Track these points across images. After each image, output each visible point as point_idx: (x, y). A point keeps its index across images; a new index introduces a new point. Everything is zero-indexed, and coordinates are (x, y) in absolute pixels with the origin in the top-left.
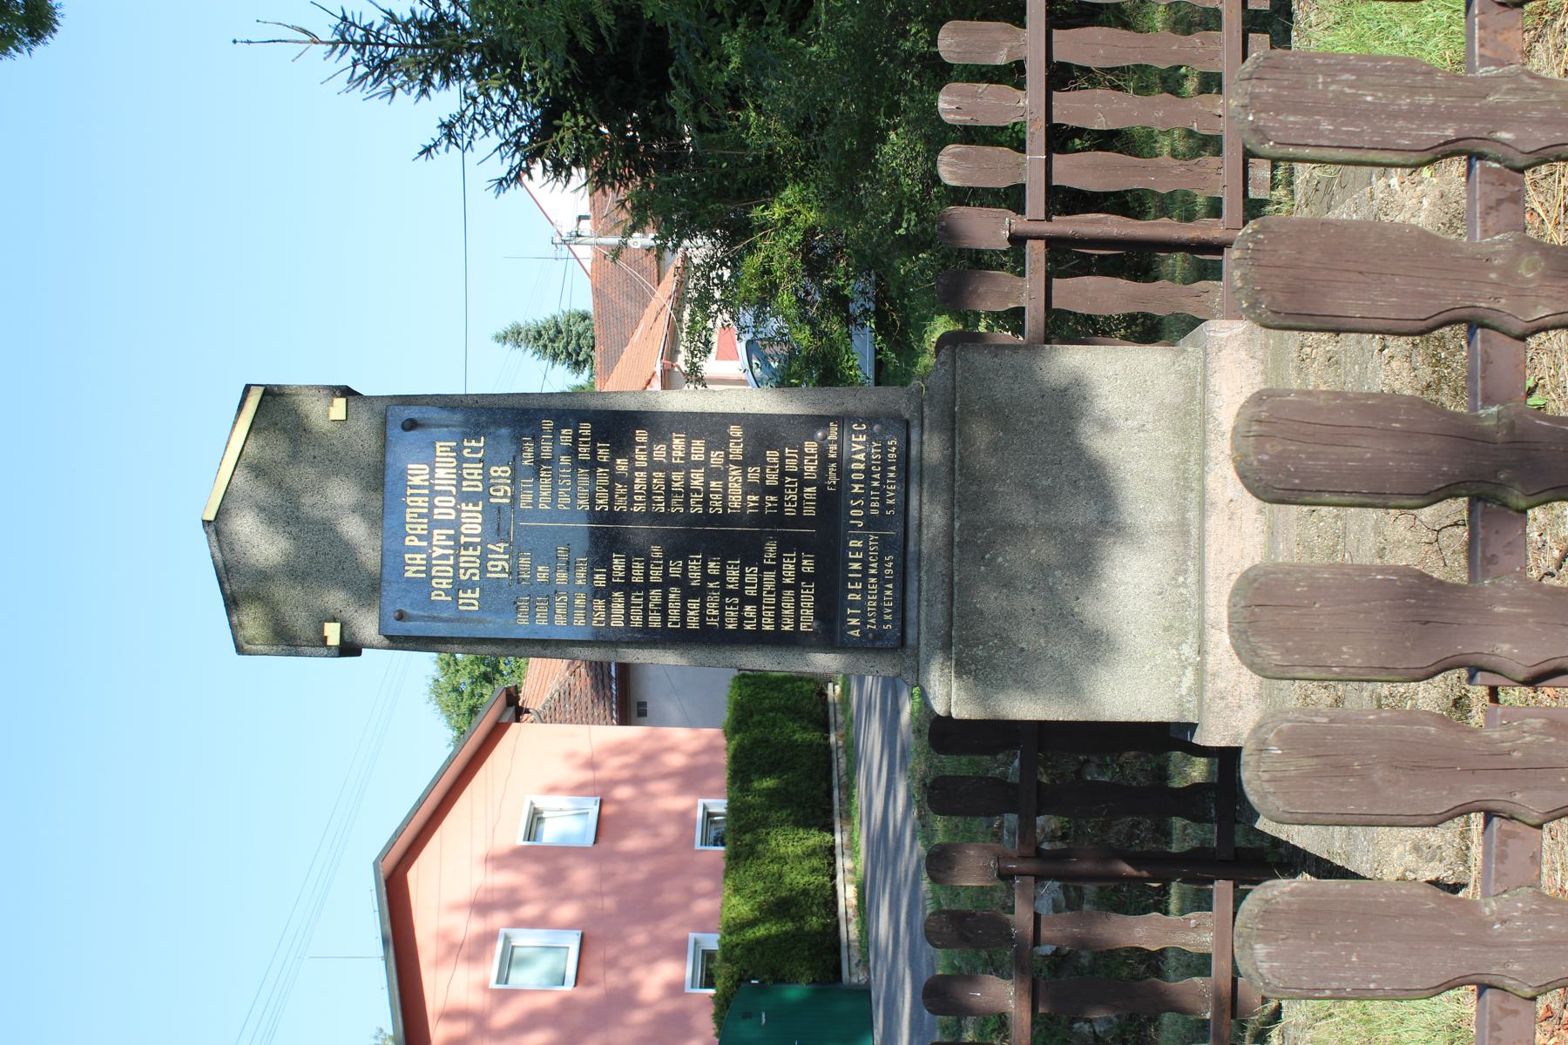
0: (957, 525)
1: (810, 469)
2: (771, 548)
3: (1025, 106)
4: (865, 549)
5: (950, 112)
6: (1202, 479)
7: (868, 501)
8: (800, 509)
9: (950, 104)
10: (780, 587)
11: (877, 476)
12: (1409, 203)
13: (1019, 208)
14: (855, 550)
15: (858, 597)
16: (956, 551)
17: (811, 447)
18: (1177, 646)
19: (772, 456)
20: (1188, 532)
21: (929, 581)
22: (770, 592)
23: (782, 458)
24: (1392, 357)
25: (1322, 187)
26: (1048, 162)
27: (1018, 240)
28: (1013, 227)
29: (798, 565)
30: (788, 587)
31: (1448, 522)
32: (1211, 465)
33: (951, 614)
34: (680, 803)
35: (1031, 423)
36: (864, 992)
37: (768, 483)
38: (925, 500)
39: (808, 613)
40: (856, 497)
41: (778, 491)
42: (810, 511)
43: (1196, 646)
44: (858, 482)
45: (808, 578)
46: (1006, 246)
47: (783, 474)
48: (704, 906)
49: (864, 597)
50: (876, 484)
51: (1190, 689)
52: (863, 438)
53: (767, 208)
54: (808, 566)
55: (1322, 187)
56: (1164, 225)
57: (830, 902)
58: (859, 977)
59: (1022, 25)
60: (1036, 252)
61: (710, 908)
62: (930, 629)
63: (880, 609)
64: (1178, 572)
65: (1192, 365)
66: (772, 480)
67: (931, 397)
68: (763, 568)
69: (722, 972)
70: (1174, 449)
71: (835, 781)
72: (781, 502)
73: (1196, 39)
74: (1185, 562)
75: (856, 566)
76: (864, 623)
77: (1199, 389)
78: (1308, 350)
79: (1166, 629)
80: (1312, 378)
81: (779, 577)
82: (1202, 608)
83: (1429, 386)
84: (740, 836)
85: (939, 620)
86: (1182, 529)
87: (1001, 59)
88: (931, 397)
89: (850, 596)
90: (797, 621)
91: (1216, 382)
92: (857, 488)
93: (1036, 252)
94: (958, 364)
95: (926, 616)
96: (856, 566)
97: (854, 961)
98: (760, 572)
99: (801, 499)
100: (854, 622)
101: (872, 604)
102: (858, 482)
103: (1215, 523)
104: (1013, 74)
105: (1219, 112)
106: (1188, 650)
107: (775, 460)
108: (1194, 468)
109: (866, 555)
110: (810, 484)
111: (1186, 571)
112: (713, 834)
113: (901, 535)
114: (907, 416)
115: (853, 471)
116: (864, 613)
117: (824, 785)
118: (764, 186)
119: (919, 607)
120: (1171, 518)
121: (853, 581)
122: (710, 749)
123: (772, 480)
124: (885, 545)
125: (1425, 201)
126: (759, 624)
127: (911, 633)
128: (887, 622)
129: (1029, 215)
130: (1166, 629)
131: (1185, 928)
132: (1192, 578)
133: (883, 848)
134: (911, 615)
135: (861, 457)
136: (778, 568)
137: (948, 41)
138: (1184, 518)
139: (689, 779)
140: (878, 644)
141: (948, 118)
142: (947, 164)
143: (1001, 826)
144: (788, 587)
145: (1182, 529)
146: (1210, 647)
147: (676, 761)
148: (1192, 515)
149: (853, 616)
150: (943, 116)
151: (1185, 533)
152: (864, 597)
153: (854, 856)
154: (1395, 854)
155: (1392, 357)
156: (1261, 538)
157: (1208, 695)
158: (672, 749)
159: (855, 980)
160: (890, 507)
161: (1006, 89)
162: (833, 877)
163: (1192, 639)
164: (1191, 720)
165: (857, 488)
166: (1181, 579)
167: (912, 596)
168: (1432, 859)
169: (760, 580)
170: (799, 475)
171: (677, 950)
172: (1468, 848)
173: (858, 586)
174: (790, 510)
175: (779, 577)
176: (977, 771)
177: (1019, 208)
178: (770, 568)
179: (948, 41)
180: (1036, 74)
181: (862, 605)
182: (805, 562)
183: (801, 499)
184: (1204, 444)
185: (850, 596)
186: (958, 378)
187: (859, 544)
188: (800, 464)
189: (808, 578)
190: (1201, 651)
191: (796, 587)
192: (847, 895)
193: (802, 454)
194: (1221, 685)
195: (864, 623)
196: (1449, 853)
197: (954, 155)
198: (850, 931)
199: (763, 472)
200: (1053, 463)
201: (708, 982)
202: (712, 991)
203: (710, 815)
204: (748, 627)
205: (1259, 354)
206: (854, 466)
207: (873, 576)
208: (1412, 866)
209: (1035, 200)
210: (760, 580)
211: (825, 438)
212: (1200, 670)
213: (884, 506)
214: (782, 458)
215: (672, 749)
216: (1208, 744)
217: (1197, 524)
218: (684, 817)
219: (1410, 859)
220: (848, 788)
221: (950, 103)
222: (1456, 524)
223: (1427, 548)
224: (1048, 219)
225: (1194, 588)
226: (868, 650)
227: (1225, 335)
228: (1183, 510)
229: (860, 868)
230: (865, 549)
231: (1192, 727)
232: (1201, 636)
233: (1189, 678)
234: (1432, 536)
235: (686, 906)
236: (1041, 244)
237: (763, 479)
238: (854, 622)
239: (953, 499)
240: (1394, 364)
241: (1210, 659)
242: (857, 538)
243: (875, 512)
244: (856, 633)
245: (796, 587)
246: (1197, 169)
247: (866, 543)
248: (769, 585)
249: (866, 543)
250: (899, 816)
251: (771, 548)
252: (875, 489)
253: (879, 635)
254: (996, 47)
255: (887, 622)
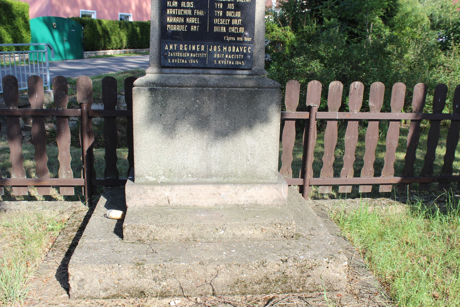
0: (210, 89)
1: (233, 30)
2: (201, 13)
3: (355, 112)
4: (200, 52)
5: (354, 86)
6: (228, 183)
7: (220, 53)
8: (217, 25)
9: (378, 87)
10: (185, 17)
11: (230, 57)
12: (338, 269)
13: (320, 110)
14: (200, 48)
15: (181, 49)
16: (200, 89)
17: (242, 30)
18: (164, 174)
19: (238, 14)
20: (208, 178)
21: (188, 77)
22: (183, 12)
23: (237, 18)
24: (279, 265)
25: (323, 212)
26: (336, 120)
27: (309, 109)
28: (314, 108)
29: (194, 24)
30: (185, 20)
31: (214, 288)
32: (234, 187)
33: (175, 87)
34: (133, 7)
35: (250, 118)
36: (82, 57)
37: (227, 12)
38: (220, 76)
39: (174, 28)
40: (222, 48)
41: (224, 16)
42: (216, 29)
43: (164, 181)
44: (227, 49)
45: (189, 28)
46: (307, 105)
47: (231, 18)
48: (106, 12)
49: (181, 51)
50: (227, 56)
51: (148, 179)
52: (245, 51)
53: (290, 31)
54: (194, 28)
55: (323, 212)
56: (312, 159)
57: (105, 48)
58: (85, 56)
59: (382, 111)
60: (304, 115)
61: (106, 16)
62: (168, 78)
63: (176, 58)
64: (192, 174)
65: (271, 178)
66: (229, 14)
67: (260, 79)
68: (193, 10)
69: (87, 18)
70: (239, 172)
71: (138, 50)
72: (220, 17)
73: (372, 169)
74: (196, 177)
75: (194, 48)
76: (171, 51)
77: (262, 181)
78: (279, 226)
79: (170, 170)
80: (268, 228)
81: (189, 16)
82: (179, 184)
83: (268, 279)
84: (123, 24)
85: (172, 82)
86: (209, 176)
87: (371, 104)
88: (260, 79)
89: (181, 45)
90: (171, 24)
91: (265, 188)
92: (225, 48)
93: (304, 115)
94: (274, 90)
95: (174, 77)
96: (194, 48)
97: (90, 55)
98: (191, 8)
99: (221, 26)
100: (171, 47)
101: (178, 54)
102: (227, 49)
103: (211, 189)
104: (365, 108)
105: (348, 177)
106: (162, 179)
107: (236, 15)
108: (232, 180)
109: (198, 52)
110: (227, 29)
111: (193, 177)
112: (123, 17)
113: (208, 66)
114: (253, 69)
115: (232, 47)
116: (175, 51)
117: (136, 47)
118: (295, 29)
119: (178, 73)
120: (213, 171)
121: (188, 47)
122: (147, 15)
123: (229, 14)
124: (202, 60)
125: (338, 274)
126: (170, 8)
127: (167, 70)
128: (171, 60)
129: (318, 113)
130: (170, 170)
131: (67, 169)
132: (190, 180)
133: (120, 61)
134: (174, 70)
135: (238, 50)
136: (193, 16)
137: (378, 86)
138: (213, 176)
139: (140, 9)
140: (162, 57)
141: (352, 85)
142: (336, 85)
143: (122, 95)
144: (185, 20)
145: (209, 176)
146: (164, 187)
147: (144, 5)
148: (214, 179)
149: (173, 47)
150: (353, 83)
151: (207, 177)
152: (181, 51)
153: (120, 54)
154: (79, 272)
155: (279, 265)
156: (206, 205)
157: (145, 187)
158: (147, 4)
159: (85, 55)
160: (217, 62)
161: (360, 105)
162: (112, 49)
163: (167, 180)
164: (136, 180)
165: (225, 48)
166: (190, 175)
167: (182, 71)
168: (79, 286)
169: (188, 8)
170: (231, 25)
171: (94, 7)
172: (84, 299)
173: (186, 49)
174: (216, 21)
175: (189, 16)
176: (114, 96)
177: (319, 110)
178: (193, 12)
179: (378, 86)
180: (365, 116)
181: (178, 50)
182: (195, 27)
183: (221, 26)
184: (241, 184)
185: (181, 45)
186: (268, 89)
187: (203, 49)
188: (235, 26)
189: (189, 28)
190: (162, 184)
191: (185, 23)
192: (110, 52)
193: (239, 26)
194: (149, 192)
195: (171, 51)
196: (82, 292)
197: (339, 87)
198: (101, 53)
199: (232, 10)
200: (235, 126)
201: (82, 16)
202: (81, 16)
203: (128, 17)
204: (168, 3)
205: (275, 203)
206: (234, 47)
207: (190, 55)
208: (75, 279)
209: (322, 115)
210: (188, 8)
211: (245, 36)
212: (155, 184)
213: (218, 60)
214: (237, 18)
215: (147, 4)
216: (126, 187)
217: (211, 181)
218: (129, 6)
219: (78, 278)
220: (136, 53)
221: (357, 86)
222: (213, 290)
223: (204, 280)
224: (316, 120)
225: (186, 180)
226: (160, 53)
227: (282, 191)
228: (216, 176)
229: (115, 56)
230: (200, 52)
231: (133, 180)
232: (168, 184)
233: (152, 179)
234: (209, 282)
235: (106, 8)
236: (308, 117)
237: (229, 10)
238: (171, 47)
239: (221, 87)
240: (277, 266)
241: (159, 188)
242: (205, 49)
243: (215, 56)
244: (167, 48)
245: (185, 23)
246: (329, 170)
247: (203, 52)
248: (186, 12)
249: (203, 52)
250: (127, 65)
251: (201, 13)
252: (225, 56)
253: (166, 57)
254: (374, 102)
255: (171, 60)
